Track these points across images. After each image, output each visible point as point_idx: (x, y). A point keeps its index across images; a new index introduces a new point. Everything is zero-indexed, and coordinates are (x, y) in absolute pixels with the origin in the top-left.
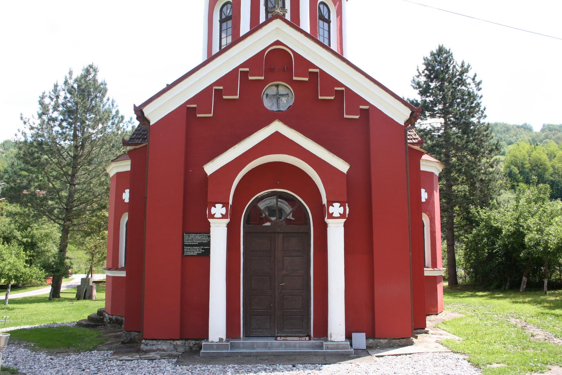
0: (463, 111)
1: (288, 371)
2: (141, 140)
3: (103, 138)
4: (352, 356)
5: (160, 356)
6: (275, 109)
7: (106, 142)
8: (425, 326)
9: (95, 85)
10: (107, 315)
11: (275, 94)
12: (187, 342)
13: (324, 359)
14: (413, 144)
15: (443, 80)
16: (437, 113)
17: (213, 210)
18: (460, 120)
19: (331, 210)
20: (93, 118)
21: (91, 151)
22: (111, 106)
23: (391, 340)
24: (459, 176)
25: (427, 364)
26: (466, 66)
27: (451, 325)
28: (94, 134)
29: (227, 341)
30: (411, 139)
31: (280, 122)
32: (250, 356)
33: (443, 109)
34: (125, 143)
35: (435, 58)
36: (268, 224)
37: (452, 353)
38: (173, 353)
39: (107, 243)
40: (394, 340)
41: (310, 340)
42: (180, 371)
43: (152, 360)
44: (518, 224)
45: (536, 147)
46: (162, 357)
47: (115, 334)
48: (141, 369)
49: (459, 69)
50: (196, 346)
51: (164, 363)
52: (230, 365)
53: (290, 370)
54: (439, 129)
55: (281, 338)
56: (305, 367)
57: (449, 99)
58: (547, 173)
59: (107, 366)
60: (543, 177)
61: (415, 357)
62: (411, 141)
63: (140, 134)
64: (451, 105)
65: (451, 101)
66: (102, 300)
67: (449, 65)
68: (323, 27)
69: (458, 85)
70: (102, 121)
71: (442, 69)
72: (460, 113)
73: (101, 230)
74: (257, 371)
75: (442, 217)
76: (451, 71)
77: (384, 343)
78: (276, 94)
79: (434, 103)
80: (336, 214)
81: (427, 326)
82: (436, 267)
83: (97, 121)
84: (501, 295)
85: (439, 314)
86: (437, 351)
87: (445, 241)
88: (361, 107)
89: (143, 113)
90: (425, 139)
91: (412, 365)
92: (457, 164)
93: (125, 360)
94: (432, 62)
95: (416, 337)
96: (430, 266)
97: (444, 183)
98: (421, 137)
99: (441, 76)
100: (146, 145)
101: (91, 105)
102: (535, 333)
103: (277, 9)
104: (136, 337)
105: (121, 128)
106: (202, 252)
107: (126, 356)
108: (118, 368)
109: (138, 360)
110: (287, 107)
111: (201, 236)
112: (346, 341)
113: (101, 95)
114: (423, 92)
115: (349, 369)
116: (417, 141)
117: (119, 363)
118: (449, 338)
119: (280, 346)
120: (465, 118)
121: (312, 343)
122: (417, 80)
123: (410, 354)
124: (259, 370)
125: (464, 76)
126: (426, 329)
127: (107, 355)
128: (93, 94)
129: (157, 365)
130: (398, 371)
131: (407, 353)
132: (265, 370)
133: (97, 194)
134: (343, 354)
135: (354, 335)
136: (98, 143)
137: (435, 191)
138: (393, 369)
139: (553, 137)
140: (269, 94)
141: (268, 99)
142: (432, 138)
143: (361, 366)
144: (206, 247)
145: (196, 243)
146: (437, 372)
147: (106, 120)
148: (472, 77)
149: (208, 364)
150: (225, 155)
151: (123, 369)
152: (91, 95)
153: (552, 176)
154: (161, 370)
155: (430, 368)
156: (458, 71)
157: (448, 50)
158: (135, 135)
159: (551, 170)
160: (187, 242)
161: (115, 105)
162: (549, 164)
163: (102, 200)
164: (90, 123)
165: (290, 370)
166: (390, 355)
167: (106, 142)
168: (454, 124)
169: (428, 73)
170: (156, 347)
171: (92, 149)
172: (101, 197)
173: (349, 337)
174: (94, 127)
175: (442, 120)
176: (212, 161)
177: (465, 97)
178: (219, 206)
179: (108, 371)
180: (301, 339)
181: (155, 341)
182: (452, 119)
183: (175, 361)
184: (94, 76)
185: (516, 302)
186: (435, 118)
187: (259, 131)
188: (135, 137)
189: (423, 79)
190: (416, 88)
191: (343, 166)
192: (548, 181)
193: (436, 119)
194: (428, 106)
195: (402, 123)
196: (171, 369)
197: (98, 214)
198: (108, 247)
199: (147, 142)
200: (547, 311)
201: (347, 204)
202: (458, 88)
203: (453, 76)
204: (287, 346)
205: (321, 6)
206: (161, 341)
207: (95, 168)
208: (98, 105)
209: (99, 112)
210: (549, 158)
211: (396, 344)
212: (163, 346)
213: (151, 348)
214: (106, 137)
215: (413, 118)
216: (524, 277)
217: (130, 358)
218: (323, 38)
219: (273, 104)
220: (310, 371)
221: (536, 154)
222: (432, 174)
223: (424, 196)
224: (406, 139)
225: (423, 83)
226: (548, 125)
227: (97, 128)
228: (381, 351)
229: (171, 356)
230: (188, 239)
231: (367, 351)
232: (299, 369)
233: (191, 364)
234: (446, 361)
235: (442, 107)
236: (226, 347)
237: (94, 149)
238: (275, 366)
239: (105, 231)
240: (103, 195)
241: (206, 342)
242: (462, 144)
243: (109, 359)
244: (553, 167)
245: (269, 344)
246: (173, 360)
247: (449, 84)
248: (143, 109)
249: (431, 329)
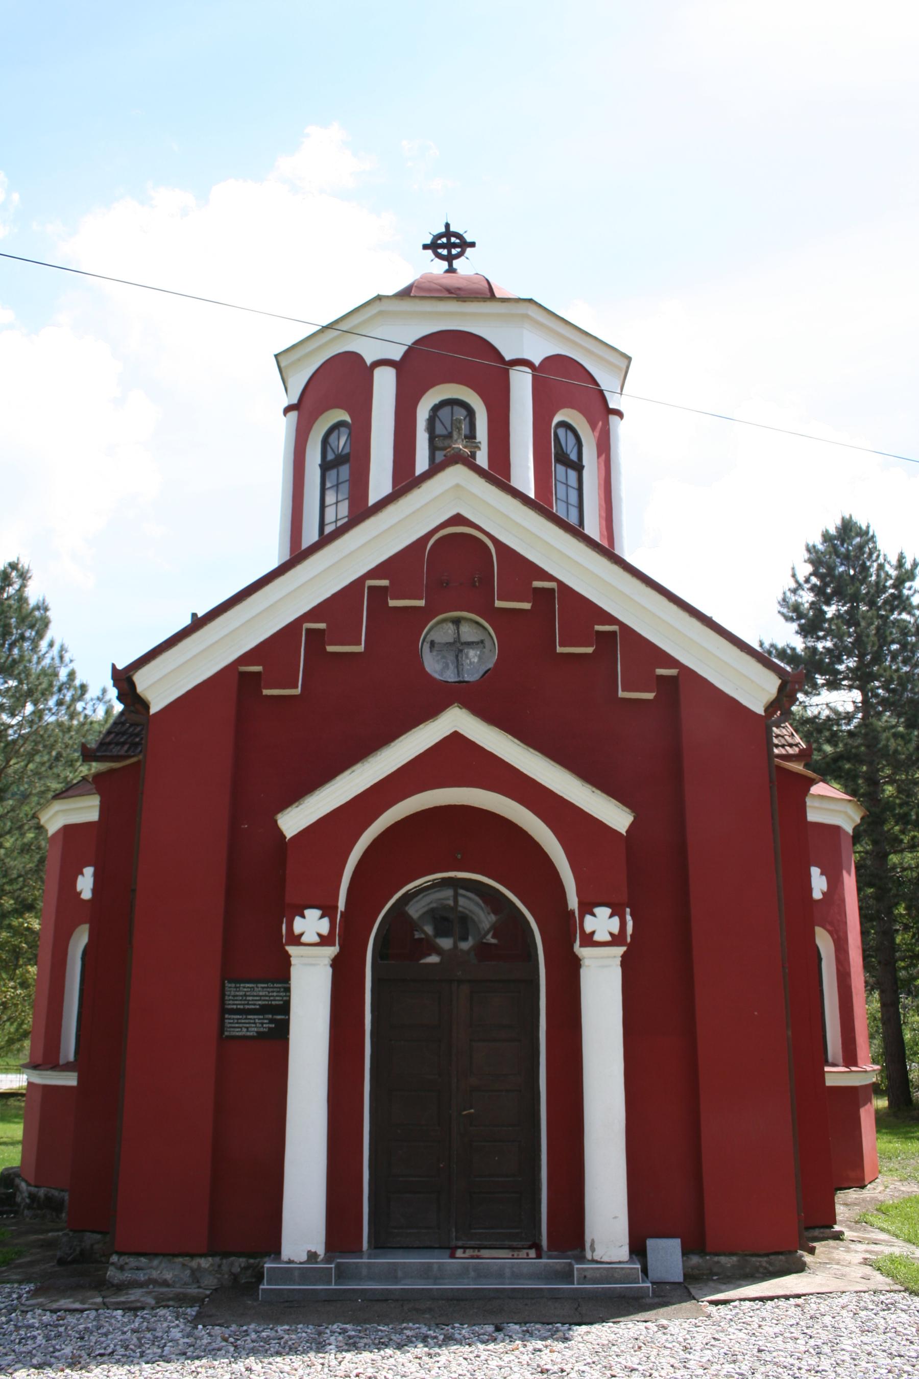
0: (906, 673)
1: (483, 1342)
2: (126, 747)
3: (34, 737)
4: (648, 1301)
5: (155, 1298)
6: (450, 676)
7: (40, 747)
8: (831, 1219)
9: (20, 611)
10: (23, 1185)
11: (452, 640)
12: (224, 1261)
13: (576, 1309)
14: (787, 757)
15: (855, 598)
16: (844, 679)
17: (299, 925)
18: (901, 696)
19: (589, 924)
20: (13, 690)
21: (5, 767)
22: (57, 661)
23: (748, 1258)
24: (903, 832)
25: (842, 1325)
26: (908, 566)
27: (900, 1215)
28: (12, 726)
29: (328, 1260)
30: (783, 746)
31: (464, 710)
32: (386, 1300)
33: (857, 669)
34: (88, 755)
35: (834, 546)
36: (434, 959)
37: (906, 1294)
38: (189, 1291)
39: (33, 997)
40: (754, 1259)
41: (539, 1256)
42: (205, 1341)
43: (132, 1309)
46: (161, 1302)
47: (41, 1237)
48: (106, 1335)
49: (893, 573)
50: (249, 1272)
51: (166, 1320)
52: (333, 1324)
53: (488, 1340)
54: (849, 717)
55: (464, 1252)
56: (527, 1331)
57: (871, 644)
59: (17, 1328)
61: (813, 1306)
62: (783, 751)
63: (123, 733)
64: (878, 658)
65: (875, 648)
66: (13, 1143)
67: (868, 564)
68: (564, 481)
69: (892, 611)
70: (35, 696)
71: (852, 572)
72: (900, 678)
73: (21, 962)
74: (403, 1343)
75: (864, 933)
76: (873, 578)
77: (729, 1265)
78: (455, 642)
79: (836, 655)
80: (602, 936)
81: (838, 1218)
82: (856, 1065)
83: (21, 696)
85: (869, 1186)
86: (865, 1289)
87: (876, 995)
88: (660, 671)
89: (133, 685)
90: (817, 741)
91: (804, 1328)
92: (898, 801)
93: (66, 1310)
94: (827, 557)
95: (812, 1251)
96: (841, 1060)
97: (868, 848)
98: (806, 737)
99: (850, 590)
100: (139, 762)
101: (10, 659)
103: (456, 441)
104: (96, 1247)
105: (79, 713)
106: (269, 1028)
107: (69, 1298)
108: (46, 1332)
109: (97, 1310)
110: (481, 673)
111: (268, 987)
112: (631, 1260)
113: (33, 633)
114: (807, 628)
115: (641, 1337)
116: (797, 749)
117: (47, 1318)
118: (896, 1251)
119: (463, 1273)
120: (912, 689)
121: (546, 1264)
122: (792, 598)
123: (798, 1296)
124: (409, 1341)
125: (904, 588)
126: (837, 1228)
127: (20, 1297)
128: (14, 631)
129: (145, 1324)
130: (768, 1345)
131: (788, 1293)
132: (424, 1340)
133: (14, 874)
134: (624, 1297)
135: (651, 1243)
136: (22, 750)
137: (845, 874)
138: (754, 1338)
140: (436, 641)
141: (435, 653)
142: (833, 739)
143: (671, 1329)
144: (279, 1017)
145: (254, 1005)
146: (869, 1348)
147: (43, 694)
149: (278, 1321)
150: (328, 790)
151: (59, 1335)
152: (11, 634)
154: (157, 1337)
155: (853, 1336)
156: (891, 578)
157: (864, 527)
158: (112, 736)
160: (231, 1002)
161: (67, 657)
163: (26, 889)
164: (5, 701)
165: (488, 1340)
166: (744, 1300)
167: (40, 747)
168: (884, 702)
169: (818, 583)
170: (145, 1274)
171: (8, 761)
172: (24, 881)
173: (638, 1249)
174: (15, 710)
175: (857, 695)
176: (296, 804)
177: (909, 639)
178: (312, 914)
179: (20, 1343)
180: (516, 1254)
181: (143, 1260)
182: (880, 691)
183: (194, 1313)
184: (19, 590)
186: (840, 689)
187: (414, 730)
188: (112, 739)
189: (807, 598)
190: (791, 619)
193: (842, 691)
194: (821, 661)
195: (760, 710)
196: (183, 1337)
197: (15, 923)
198: (34, 1006)
199: (141, 752)
201: (628, 910)
202: (892, 618)
203: (880, 588)
204: (481, 1274)
205: (561, 432)
206: (161, 1258)
207: (13, 809)
208: (27, 658)
209: (28, 675)
211: (761, 1270)
212: (164, 1272)
213: (134, 1277)
214: (42, 736)
215: (786, 697)
217: (77, 1306)
218: (564, 505)
219: (446, 666)
220: (539, 1344)
222: (836, 830)
223: (819, 884)
224: (771, 745)
225: (807, 605)
227: (20, 712)
228: (723, 1287)
229: (182, 1300)
230: (234, 996)
231: (686, 1288)
232: (511, 1337)
233: (234, 1322)
234: (892, 1318)
235: (855, 664)
236: (324, 1276)
237: (12, 762)
238: (449, 1327)
239: (29, 967)
240: (29, 876)
241: (273, 1261)
242: (907, 752)
243: (24, 1309)
245: (435, 1267)
246: (189, 1310)
247: (871, 608)
248: (134, 674)
249: (851, 1228)
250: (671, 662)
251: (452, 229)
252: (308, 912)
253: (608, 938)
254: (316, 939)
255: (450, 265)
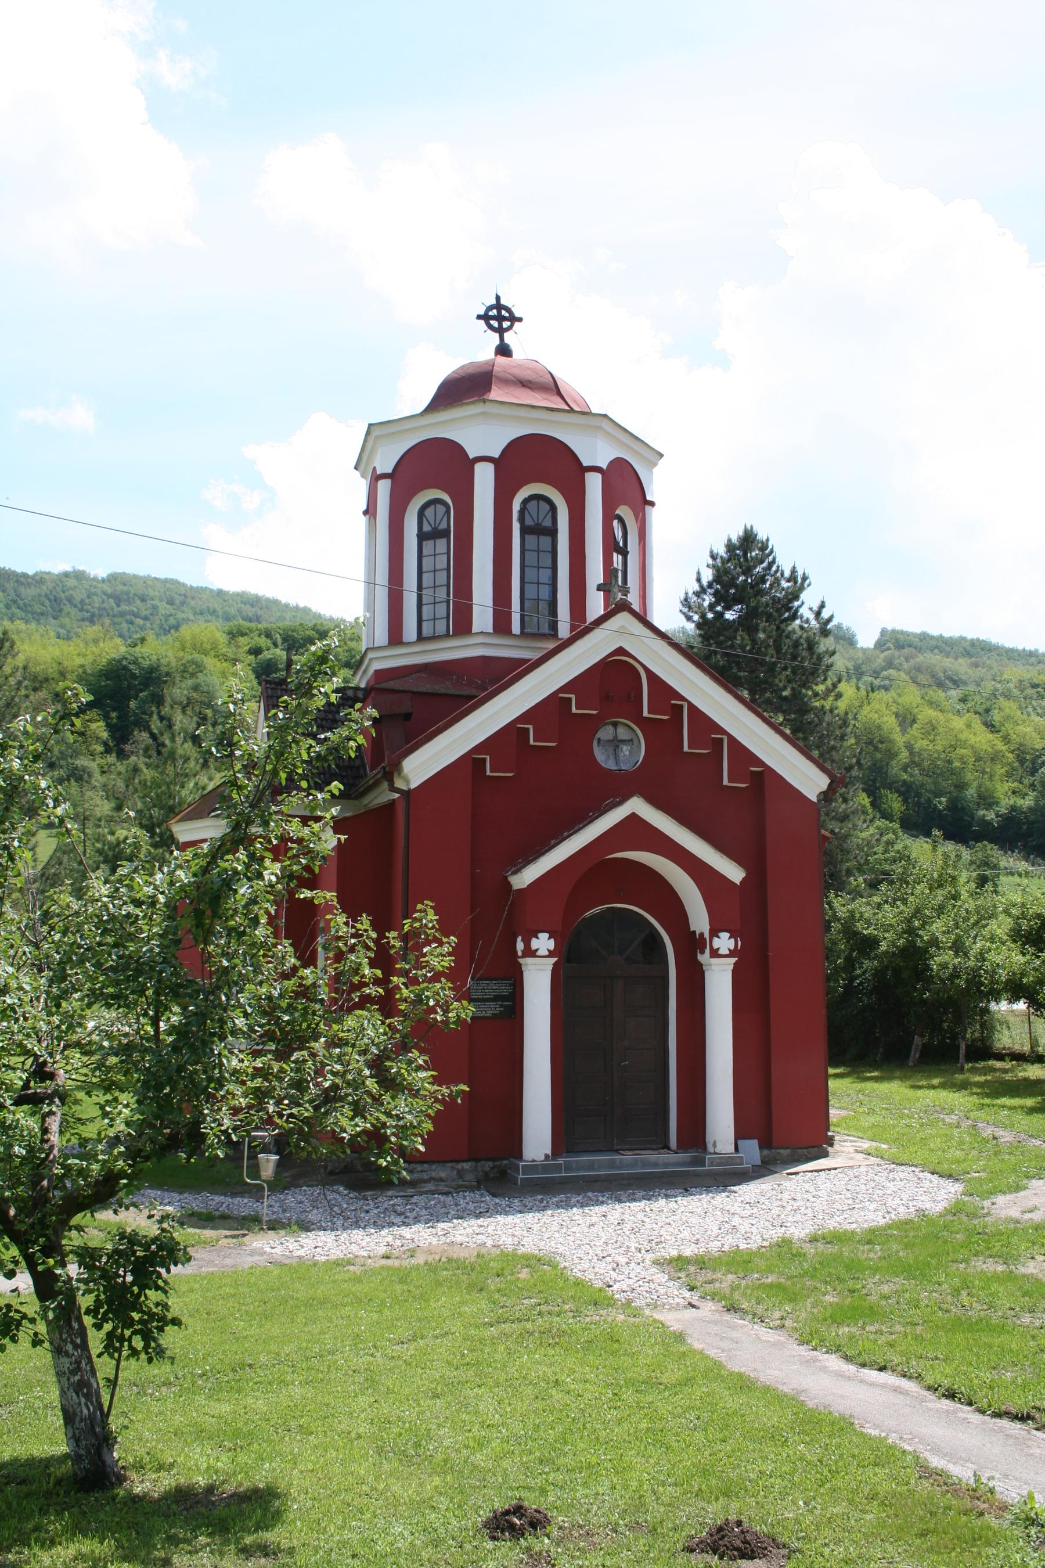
19: (717, 943)
44: (911, 931)
45: (871, 694)
50: (495, 1170)
58: (894, 763)
60: (886, 773)
80: (724, 951)
84: (876, 1074)
102: (997, 1135)
139: (906, 666)
148: (815, 608)
153: (906, 771)
159: (904, 755)
162: (900, 740)
178: (544, 936)
185: (920, 1087)
189: (708, 600)
191: (734, 873)
192: (896, 782)
200: (987, 1101)
204: (645, 1164)
210: (900, 725)
216: (916, 1037)
221: (871, 715)
226: (893, 631)
244: (909, 747)
250: (761, 763)
251: (503, 302)
252: (540, 935)
253: (728, 952)
254: (547, 953)
255: (502, 338)
